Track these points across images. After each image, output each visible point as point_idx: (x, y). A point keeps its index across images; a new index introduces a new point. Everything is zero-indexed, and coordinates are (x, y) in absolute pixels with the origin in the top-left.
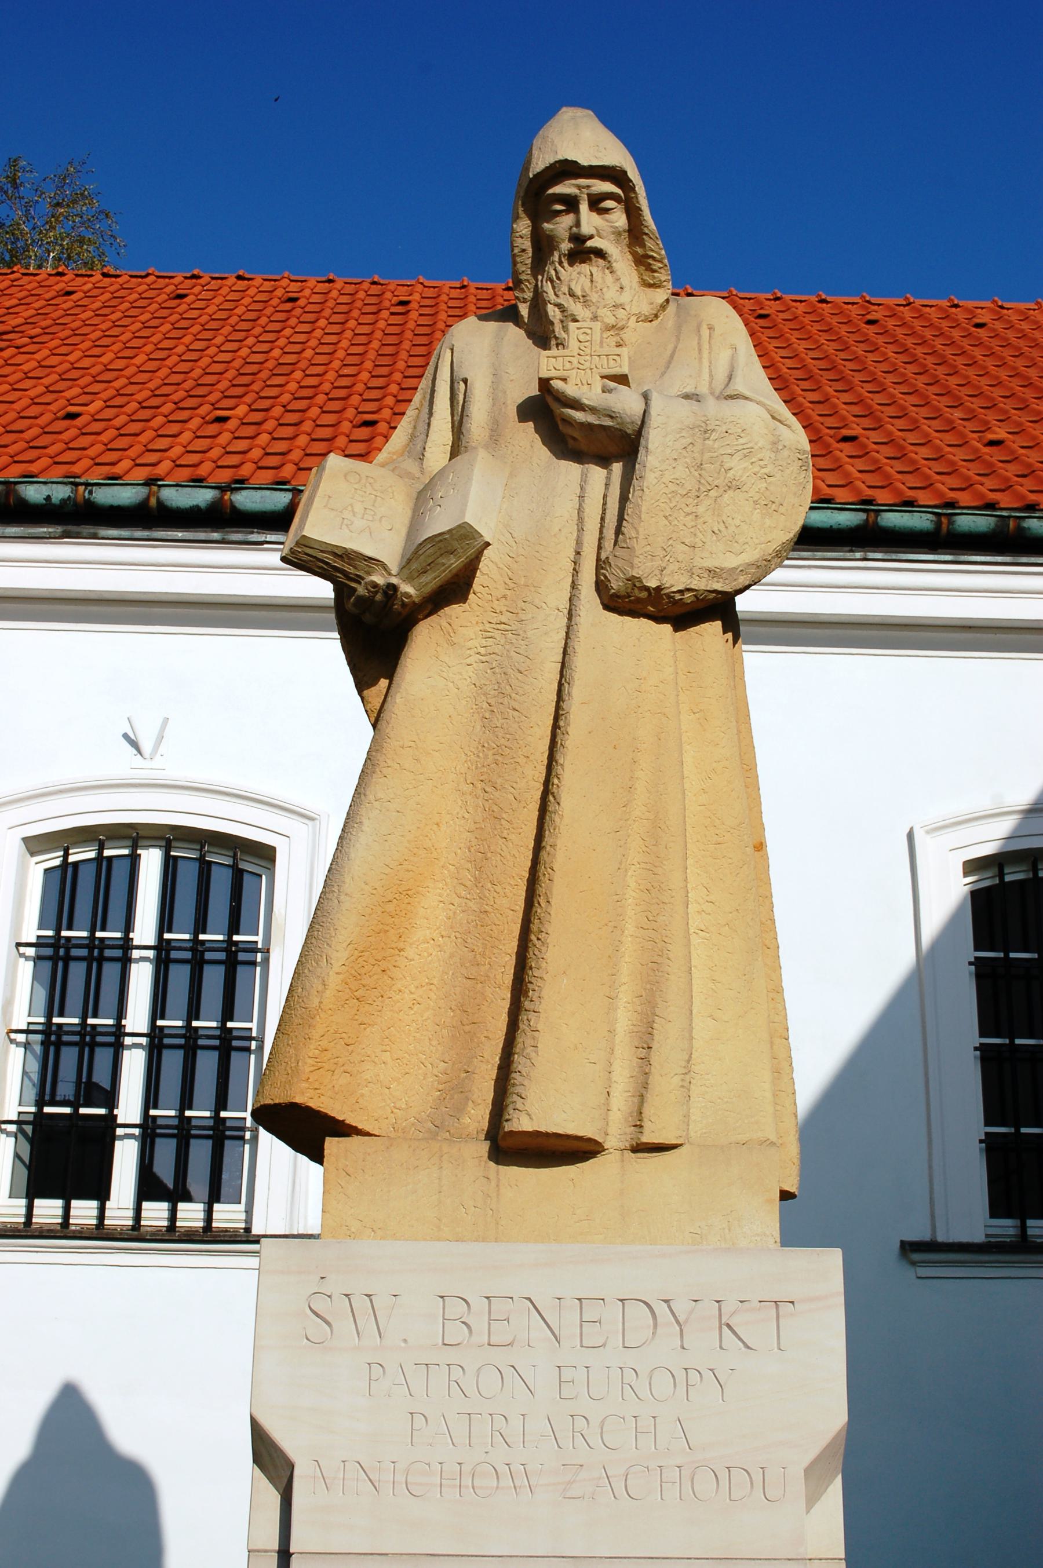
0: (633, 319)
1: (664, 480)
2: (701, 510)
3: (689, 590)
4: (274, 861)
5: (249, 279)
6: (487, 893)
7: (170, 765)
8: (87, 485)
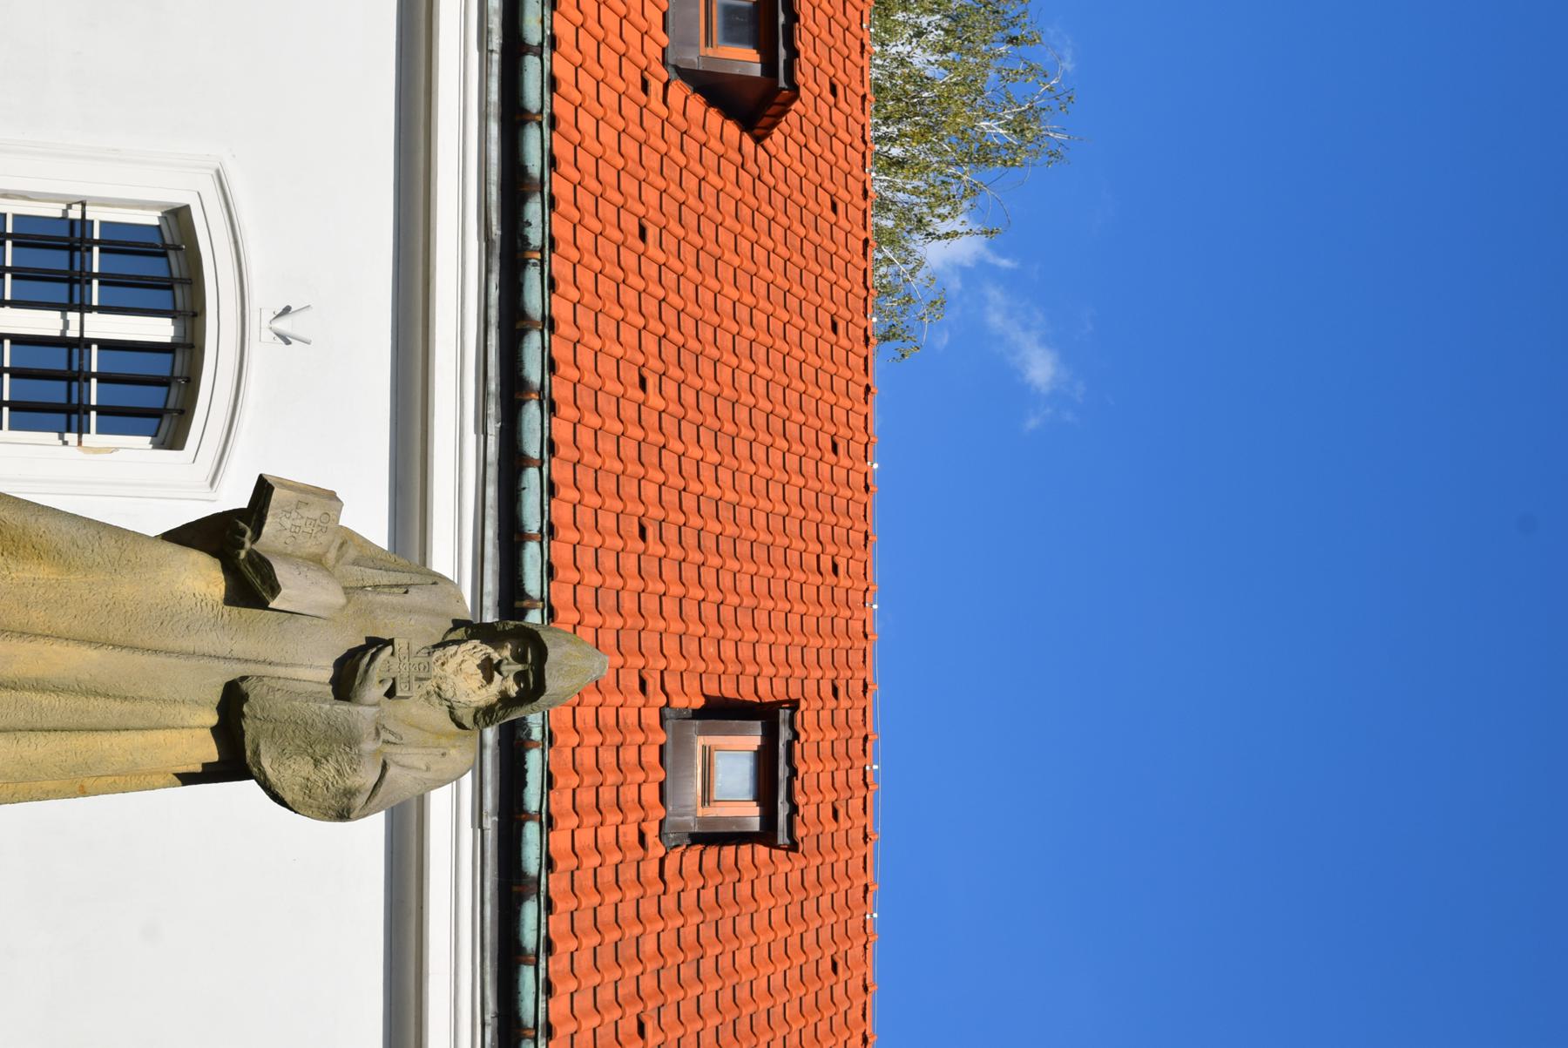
4: (171, 448)
7: (262, 348)
8: (542, 261)
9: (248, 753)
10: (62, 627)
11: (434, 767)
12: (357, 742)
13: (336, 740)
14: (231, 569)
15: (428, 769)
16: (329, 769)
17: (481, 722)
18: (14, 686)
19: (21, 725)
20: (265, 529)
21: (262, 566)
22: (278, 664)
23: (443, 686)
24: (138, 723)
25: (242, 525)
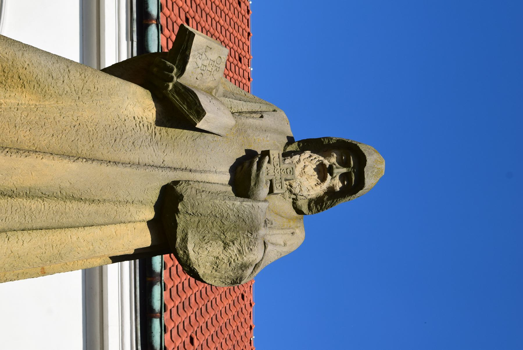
0: (294, 197)
1: (229, 210)
5: (248, 38)
6: (25, 127)
9: (178, 240)
10: (43, 143)
11: (288, 243)
12: (257, 230)
13: (242, 229)
14: (159, 97)
15: (285, 245)
16: (233, 250)
17: (314, 210)
18: (11, 194)
19: (16, 226)
20: (188, 67)
21: (189, 96)
22: (195, 171)
23: (294, 185)
24: (101, 220)
25: (168, 63)
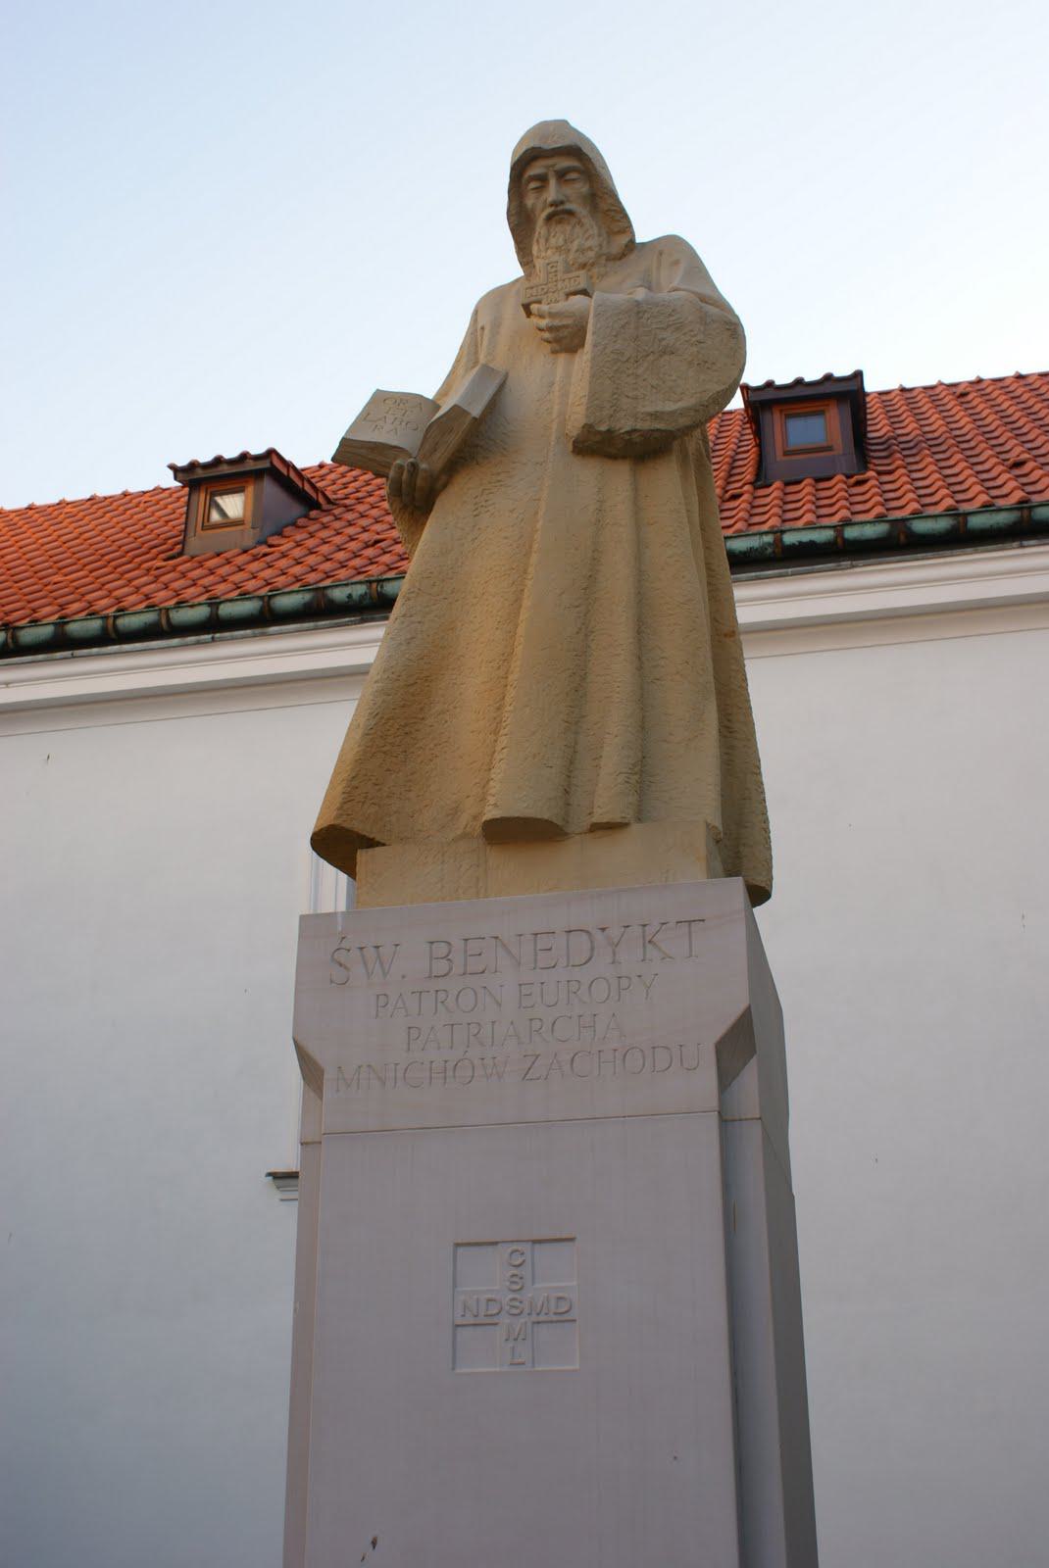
2: (640, 371)
3: (635, 431)
